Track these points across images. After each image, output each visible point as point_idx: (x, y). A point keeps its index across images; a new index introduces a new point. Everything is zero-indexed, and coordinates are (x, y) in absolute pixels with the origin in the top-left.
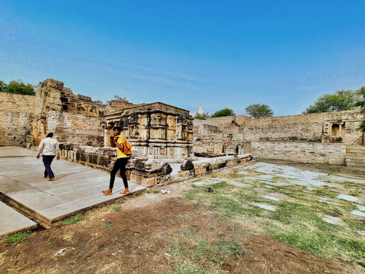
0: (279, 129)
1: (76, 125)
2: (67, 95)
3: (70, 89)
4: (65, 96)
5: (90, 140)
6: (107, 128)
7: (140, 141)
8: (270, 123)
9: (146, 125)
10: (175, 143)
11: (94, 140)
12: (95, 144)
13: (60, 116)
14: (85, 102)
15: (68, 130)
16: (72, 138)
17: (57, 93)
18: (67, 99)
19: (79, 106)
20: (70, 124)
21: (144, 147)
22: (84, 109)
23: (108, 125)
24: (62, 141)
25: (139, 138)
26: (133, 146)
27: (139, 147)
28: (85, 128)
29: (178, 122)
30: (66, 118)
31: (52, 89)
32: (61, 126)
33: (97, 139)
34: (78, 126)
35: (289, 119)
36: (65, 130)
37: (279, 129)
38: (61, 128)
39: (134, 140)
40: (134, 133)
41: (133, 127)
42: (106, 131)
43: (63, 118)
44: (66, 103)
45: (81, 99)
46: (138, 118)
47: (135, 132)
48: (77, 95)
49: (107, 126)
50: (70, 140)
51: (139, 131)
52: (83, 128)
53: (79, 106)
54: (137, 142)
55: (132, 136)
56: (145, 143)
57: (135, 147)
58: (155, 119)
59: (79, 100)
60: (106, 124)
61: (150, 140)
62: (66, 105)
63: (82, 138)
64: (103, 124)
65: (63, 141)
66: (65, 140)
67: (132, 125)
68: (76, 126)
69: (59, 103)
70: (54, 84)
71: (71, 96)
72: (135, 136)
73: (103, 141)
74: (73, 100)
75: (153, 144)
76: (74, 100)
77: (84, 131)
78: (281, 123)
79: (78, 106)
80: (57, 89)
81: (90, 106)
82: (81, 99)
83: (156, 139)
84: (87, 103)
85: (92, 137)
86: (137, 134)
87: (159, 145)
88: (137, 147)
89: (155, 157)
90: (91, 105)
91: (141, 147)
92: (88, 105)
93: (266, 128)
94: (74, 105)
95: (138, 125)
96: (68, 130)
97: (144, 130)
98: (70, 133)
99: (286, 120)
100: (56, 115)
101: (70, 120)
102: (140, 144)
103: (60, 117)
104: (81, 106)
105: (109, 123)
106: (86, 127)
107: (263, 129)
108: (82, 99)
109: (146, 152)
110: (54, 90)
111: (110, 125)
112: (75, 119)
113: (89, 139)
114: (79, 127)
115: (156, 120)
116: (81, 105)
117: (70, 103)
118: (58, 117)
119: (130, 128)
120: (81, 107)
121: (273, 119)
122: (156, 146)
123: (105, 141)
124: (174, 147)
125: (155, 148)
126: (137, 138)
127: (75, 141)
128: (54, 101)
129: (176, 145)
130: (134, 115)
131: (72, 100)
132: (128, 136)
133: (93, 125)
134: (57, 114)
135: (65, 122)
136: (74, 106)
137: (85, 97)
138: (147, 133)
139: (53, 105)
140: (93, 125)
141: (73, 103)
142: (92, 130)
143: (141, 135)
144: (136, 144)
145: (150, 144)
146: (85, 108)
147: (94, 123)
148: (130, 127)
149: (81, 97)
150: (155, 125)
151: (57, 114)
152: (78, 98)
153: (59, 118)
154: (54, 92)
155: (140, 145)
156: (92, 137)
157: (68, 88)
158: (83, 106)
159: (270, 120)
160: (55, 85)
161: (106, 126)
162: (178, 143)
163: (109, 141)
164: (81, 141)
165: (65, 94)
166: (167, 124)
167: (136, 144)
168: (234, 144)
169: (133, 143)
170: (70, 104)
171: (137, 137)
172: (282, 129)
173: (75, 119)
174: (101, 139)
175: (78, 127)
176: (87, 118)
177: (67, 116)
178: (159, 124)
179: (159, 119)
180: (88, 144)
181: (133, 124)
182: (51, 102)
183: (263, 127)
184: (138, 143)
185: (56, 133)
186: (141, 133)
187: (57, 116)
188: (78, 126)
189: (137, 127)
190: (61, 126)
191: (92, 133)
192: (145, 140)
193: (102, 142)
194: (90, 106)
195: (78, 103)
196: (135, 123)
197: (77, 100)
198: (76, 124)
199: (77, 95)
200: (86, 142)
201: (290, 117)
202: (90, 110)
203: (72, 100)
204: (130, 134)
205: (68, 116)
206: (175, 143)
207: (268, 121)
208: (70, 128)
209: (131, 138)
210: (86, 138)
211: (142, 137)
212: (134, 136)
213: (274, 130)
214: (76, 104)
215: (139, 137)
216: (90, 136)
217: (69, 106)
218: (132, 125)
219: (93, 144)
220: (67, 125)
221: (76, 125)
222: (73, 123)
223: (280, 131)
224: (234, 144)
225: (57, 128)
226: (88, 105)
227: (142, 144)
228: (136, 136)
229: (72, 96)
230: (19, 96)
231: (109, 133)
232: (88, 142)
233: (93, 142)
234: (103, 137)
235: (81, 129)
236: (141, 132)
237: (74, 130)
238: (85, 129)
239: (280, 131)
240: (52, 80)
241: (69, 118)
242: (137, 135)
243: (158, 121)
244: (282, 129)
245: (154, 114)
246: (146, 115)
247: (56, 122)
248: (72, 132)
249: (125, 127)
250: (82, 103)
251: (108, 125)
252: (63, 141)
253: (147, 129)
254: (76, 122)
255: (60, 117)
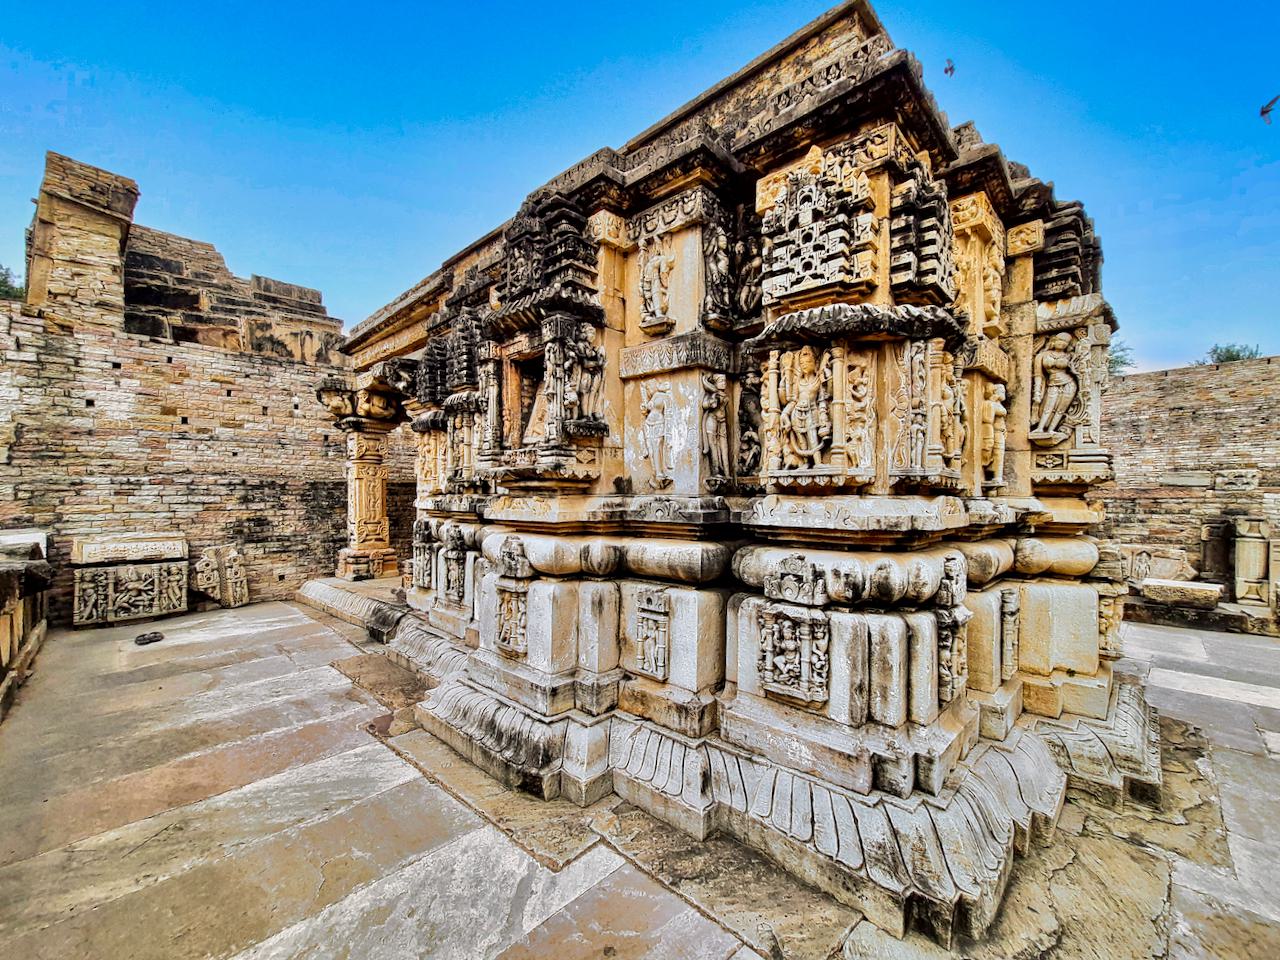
0: (1247, 421)
1: (168, 411)
2: (197, 275)
3: (211, 247)
4: (181, 281)
5: (254, 506)
6: (357, 427)
7: (622, 525)
8: (1152, 401)
9: (687, 321)
10: (1016, 529)
11: (282, 507)
12: (288, 532)
13: (47, 349)
14: (290, 316)
15: (114, 444)
16: (117, 493)
17: (97, 238)
18: (196, 298)
19: (259, 334)
20: (124, 407)
21: (674, 593)
22: (285, 346)
23: (366, 406)
24: (30, 520)
25: (599, 489)
26: (537, 575)
27: (608, 587)
28: (238, 430)
29: (1038, 285)
30: (90, 364)
31: (62, 210)
32: (51, 418)
33: (304, 498)
34: (185, 421)
35: (1265, 376)
36: (86, 445)
37: (1247, 421)
38: (57, 430)
39: (555, 510)
40: (544, 427)
41: (531, 369)
42: (354, 443)
43: (67, 366)
44: (187, 318)
45: (268, 299)
46: (584, 249)
47: (554, 408)
48: (249, 278)
49: (361, 412)
50: (94, 513)
51: (602, 405)
52: (219, 431)
53: (259, 334)
54: (583, 529)
55: (523, 463)
56: (692, 552)
57: (569, 586)
58: (852, 210)
59: (257, 301)
60: (351, 399)
61: (770, 512)
62: (191, 325)
63: (191, 492)
64: (336, 401)
65: (39, 518)
66: (49, 516)
67: (522, 343)
68: (171, 418)
69: (106, 297)
70: (70, 181)
71: (215, 281)
72: (558, 466)
73: (345, 506)
74: (229, 304)
75: (826, 561)
76: (233, 302)
77: (232, 447)
78: (1213, 394)
79: (252, 334)
80: (76, 203)
81: (316, 336)
82: (268, 299)
83: (861, 490)
84: (301, 317)
85: (272, 485)
86: (586, 432)
87: (902, 571)
88: (589, 589)
89: (878, 765)
90: (321, 329)
91: (631, 589)
92: (304, 328)
93: (1155, 420)
94: (233, 328)
95: (589, 330)
96: (114, 444)
97: (666, 383)
98: (126, 467)
99: (1244, 382)
100: (10, 342)
101: (122, 376)
102: (621, 555)
103: (43, 357)
104: (268, 335)
105: (371, 392)
106: (240, 426)
107: (1135, 426)
108: (275, 300)
109: (711, 659)
110: (77, 219)
111: (377, 406)
112: (162, 374)
113: (245, 500)
114: (195, 423)
115: (864, 219)
116: (269, 326)
117: (212, 316)
118: (30, 355)
119: (499, 375)
120: (271, 339)
121: (1169, 378)
122: (883, 600)
123: (351, 510)
124: (1017, 573)
125: (874, 621)
126: (583, 487)
127: (138, 515)
128: (77, 281)
129: (1042, 551)
130: (550, 225)
131: (220, 300)
132: (487, 467)
133: (291, 415)
134: (19, 333)
135: (90, 394)
136: (235, 332)
137: (289, 290)
138: (711, 423)
139: (65, 305)
140: (291, 415)
141: (229, 317)
142: (283, 445)
143: (629, 455)
144: (571, 550)
145: (761, 562)
146: (289, 341)
147: (296, 400)
148: (499, 364)
149: (267, 289)
150: (842, 291)
151: (19, 333)
152: (255, 294)
153: (39, 362)
154: (75, 232)
155: (620, 570)
156: (274, 487)
157: (202, 244)
158: (280, 332)
159: (1148, 388)
160: (82, 188)
161: (354, 414)
162: (1050, 531)
163: (379, 509)
164: (183, 512)
165: (186, 272)
166: (1018, 262)
167: (571, 550)
168: (1177, 508)
169: (541, 549)
170: (209, 321)
171: (588, 479)
172: (1266, 420)
173: (162, 374)
174: (330, 496)
175: (185, 427)
176: (249, 371)
177: (101, 351)
178: (901, 278)
179: (894, 214)
180: (241, 532)
181: (532, 329)
182: (55, 287)
183: (1135, 418)
184: (599, 548)
185: (15, 462)
186: (629, 430)
187: (19, 346)
188: (185, 421)
189: (581, 360)
190: (57, 420)
191: (276, 463)
192: (694, 506)
193: (337, 518)
194: (316, 331)
195: (254, 317)
196: (556, 304)
197: (248, 304)
198: (169, 404)
199: (249, 278)
200: (222, 521)
201: (1272, 366)
202: (315, 351)
203: (220, 300)
204: (500, 440)
205: (110, 352)
206: (1016, 529)
207: (1135, 390)
208: (126, 431)
209: (523, 482)
210: (224, 490)
211: (636, 472)
212: (545, 462)
213: (1207, 427)
214: (243, 324)
215: (603, 468)
216: (256, 481)
217: (207, 330)
218: (522, 343)
219: (277, 532)
220: (102, 413)
221: (168, 411)
222: (147, 396)
223: (1249, 431)
224: (1177, 508)
225: (19, 431)
226: (304, 328)
227: (651, 552)
228: (574, 467)
229: (225, 281)
230: (13, 306)
231: (379, 460)
232: (240, 522)
233: (275, 521)
234: (342, 485)
235: (206, 436)
236: (621, 421)
237: (156, 444)
238: (232, 440)
239: (1249, 431)
240: (62, 159)
241: (117, 366)
242: (584, 455)
243: (884, 243)
244: (1266, 420)
245: (816, 151)
246: (695, 202)
247: (15, 394)
248: (143, 457)
249: (460, 387)
250: (275, 317)
251: (363, 407)
252: (39, 518)
253: (705, 368)
254: (172, 393)
255: (43, 357)
